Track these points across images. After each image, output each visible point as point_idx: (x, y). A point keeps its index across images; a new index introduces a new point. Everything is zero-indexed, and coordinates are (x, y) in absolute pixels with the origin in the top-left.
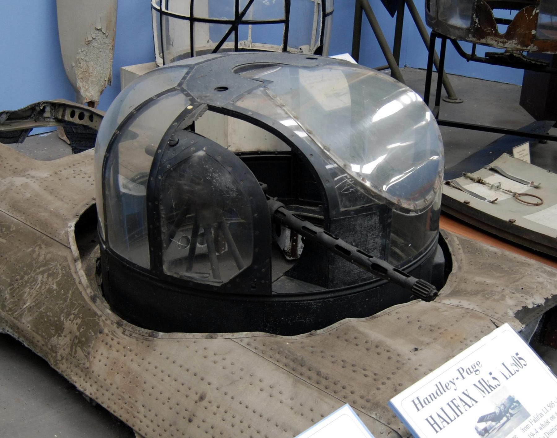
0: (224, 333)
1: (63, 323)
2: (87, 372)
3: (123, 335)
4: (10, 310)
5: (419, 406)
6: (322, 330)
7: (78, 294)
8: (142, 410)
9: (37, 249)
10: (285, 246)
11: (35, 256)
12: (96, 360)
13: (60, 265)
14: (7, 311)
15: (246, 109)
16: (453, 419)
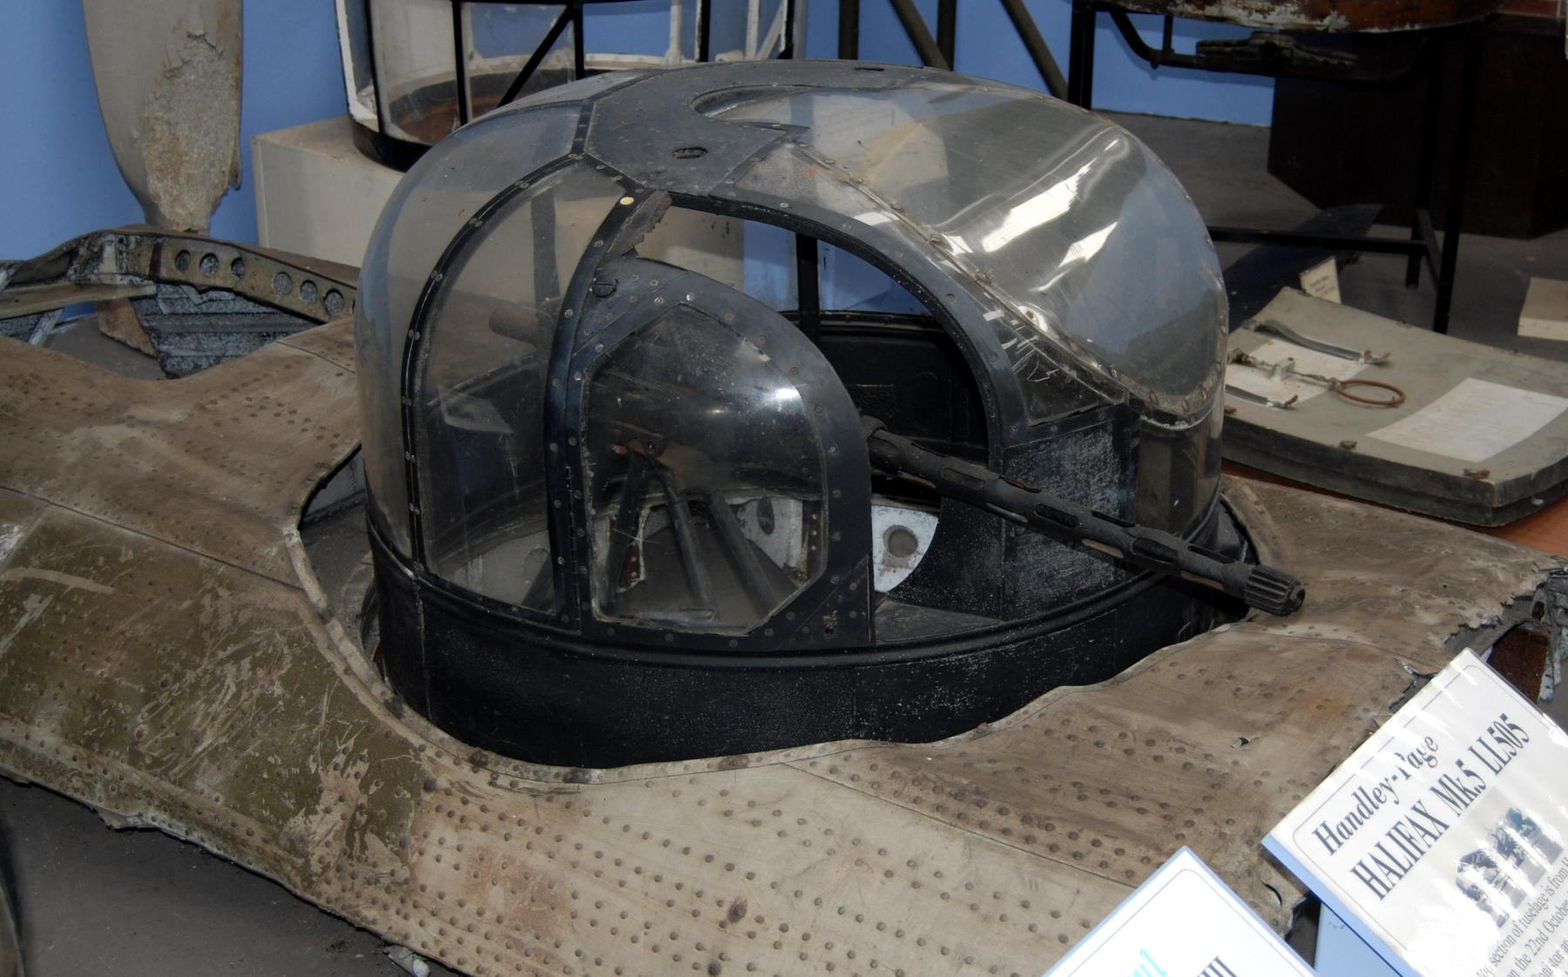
0: (763, 754)
1: (316, 778)
2: (406, 891)
3: (491, 789)
4: (157, 762)
5: (1331, 842)
6: (1003, 721)
7: (346, 701)
9: (207, 600)
10: (789, 557)
11: (204, 619)
12: (428, 861)
13: (283, 634)
14: (149, 767)
15: (773, 197)
16: (1406, 866)
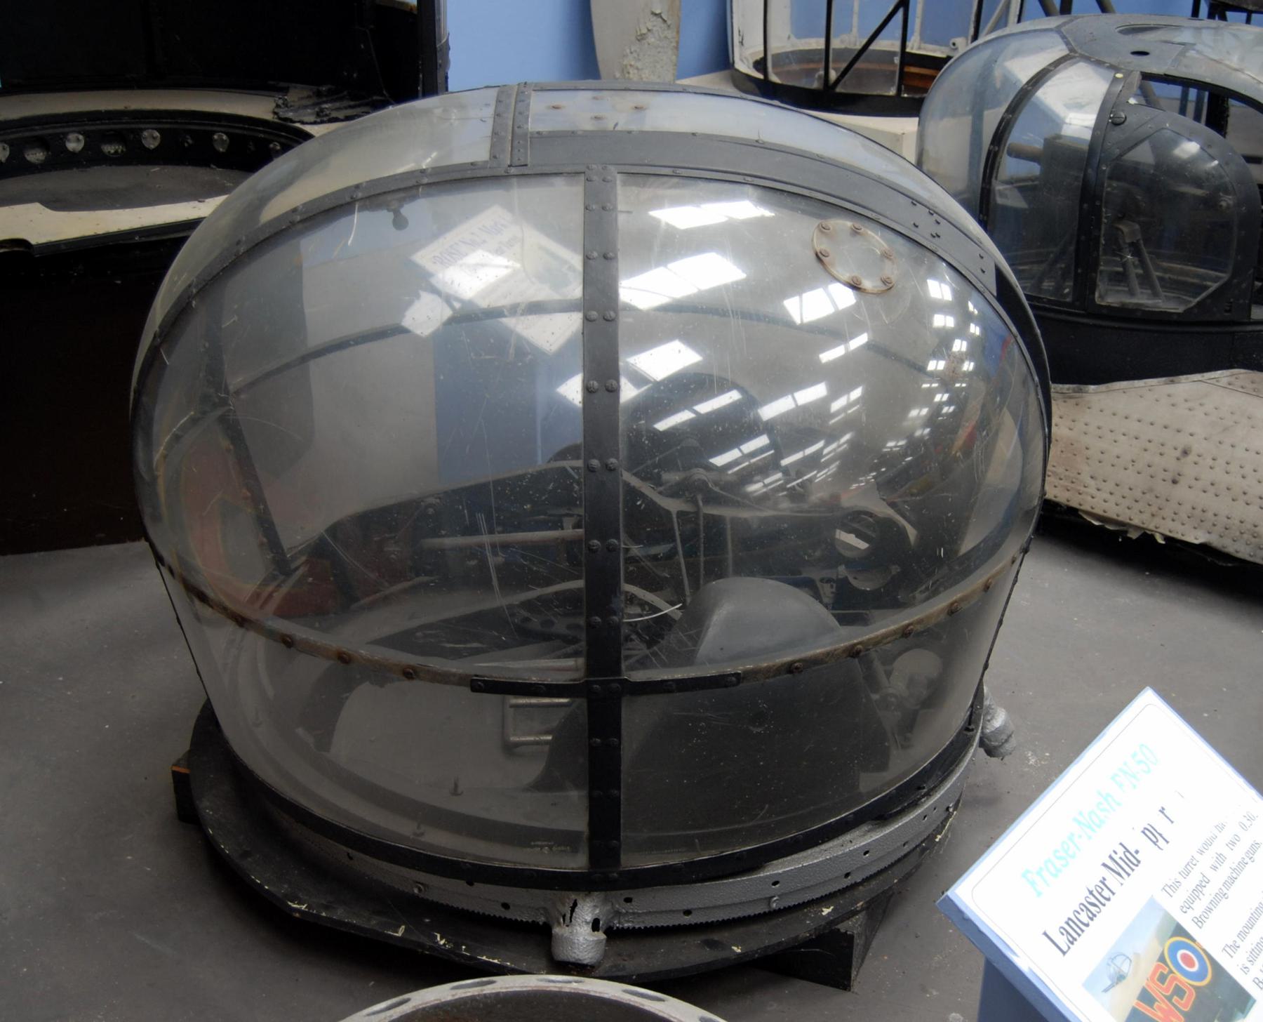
8: (1092, 483)
16: (1065, 949)
